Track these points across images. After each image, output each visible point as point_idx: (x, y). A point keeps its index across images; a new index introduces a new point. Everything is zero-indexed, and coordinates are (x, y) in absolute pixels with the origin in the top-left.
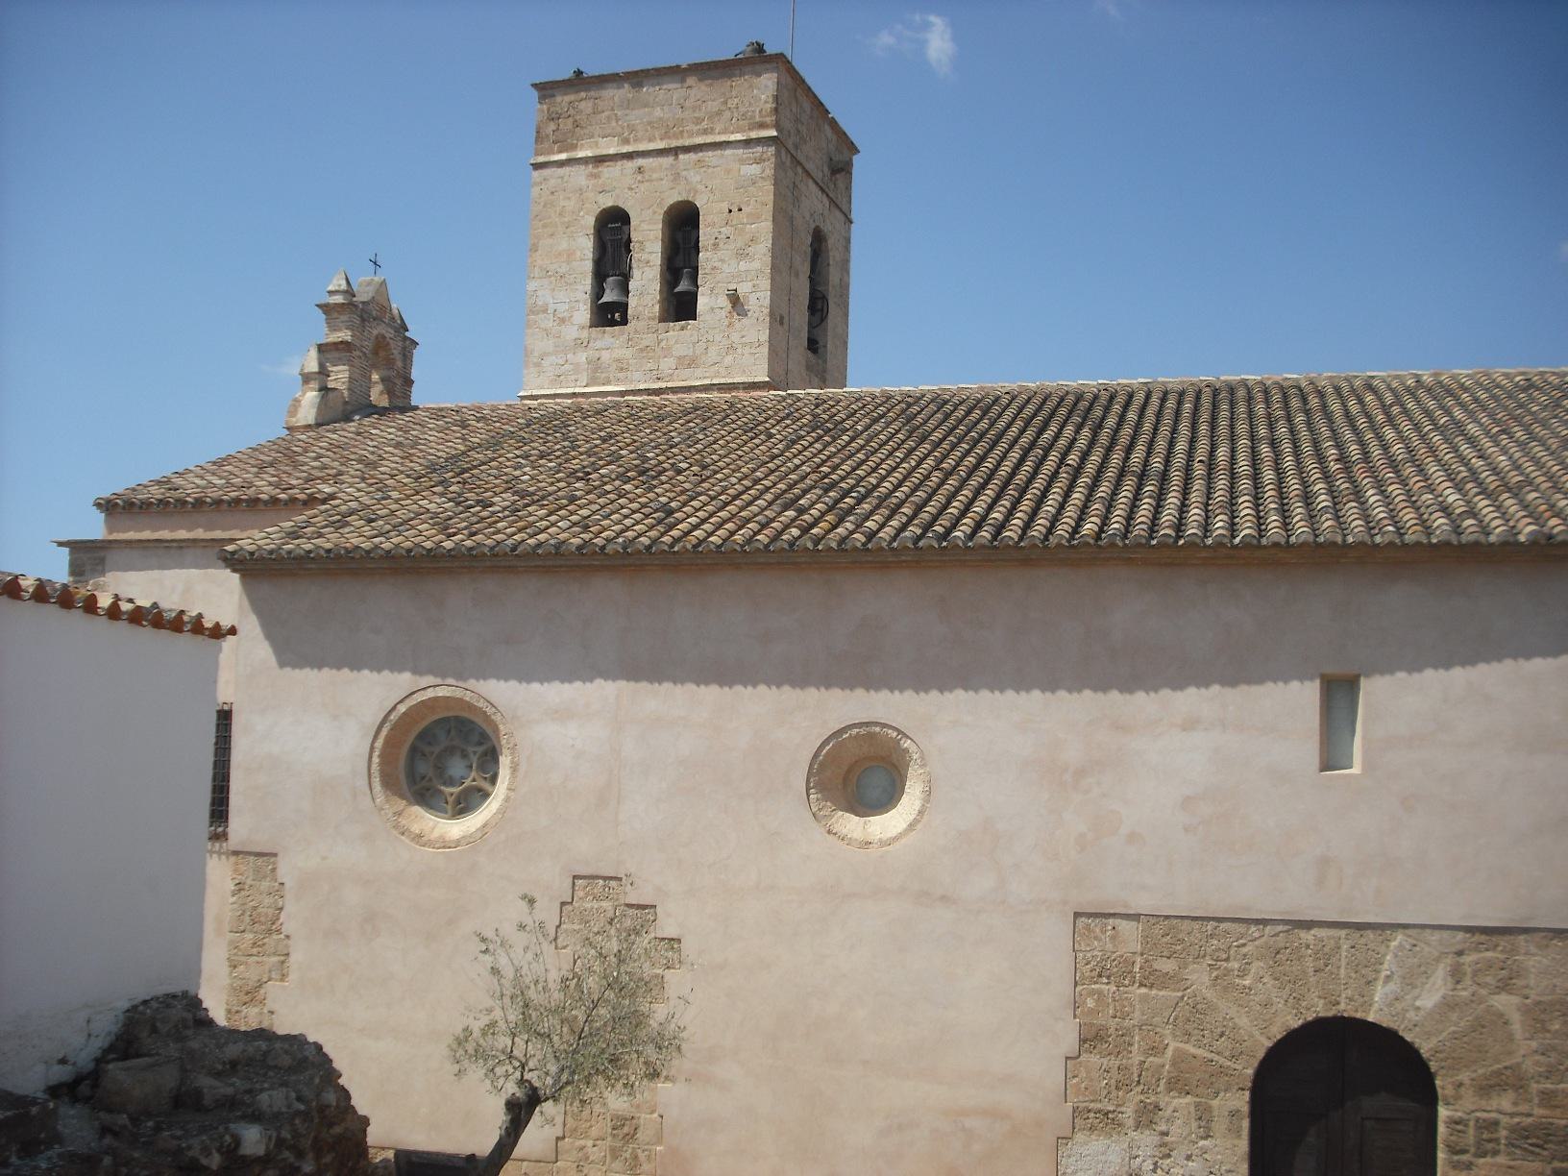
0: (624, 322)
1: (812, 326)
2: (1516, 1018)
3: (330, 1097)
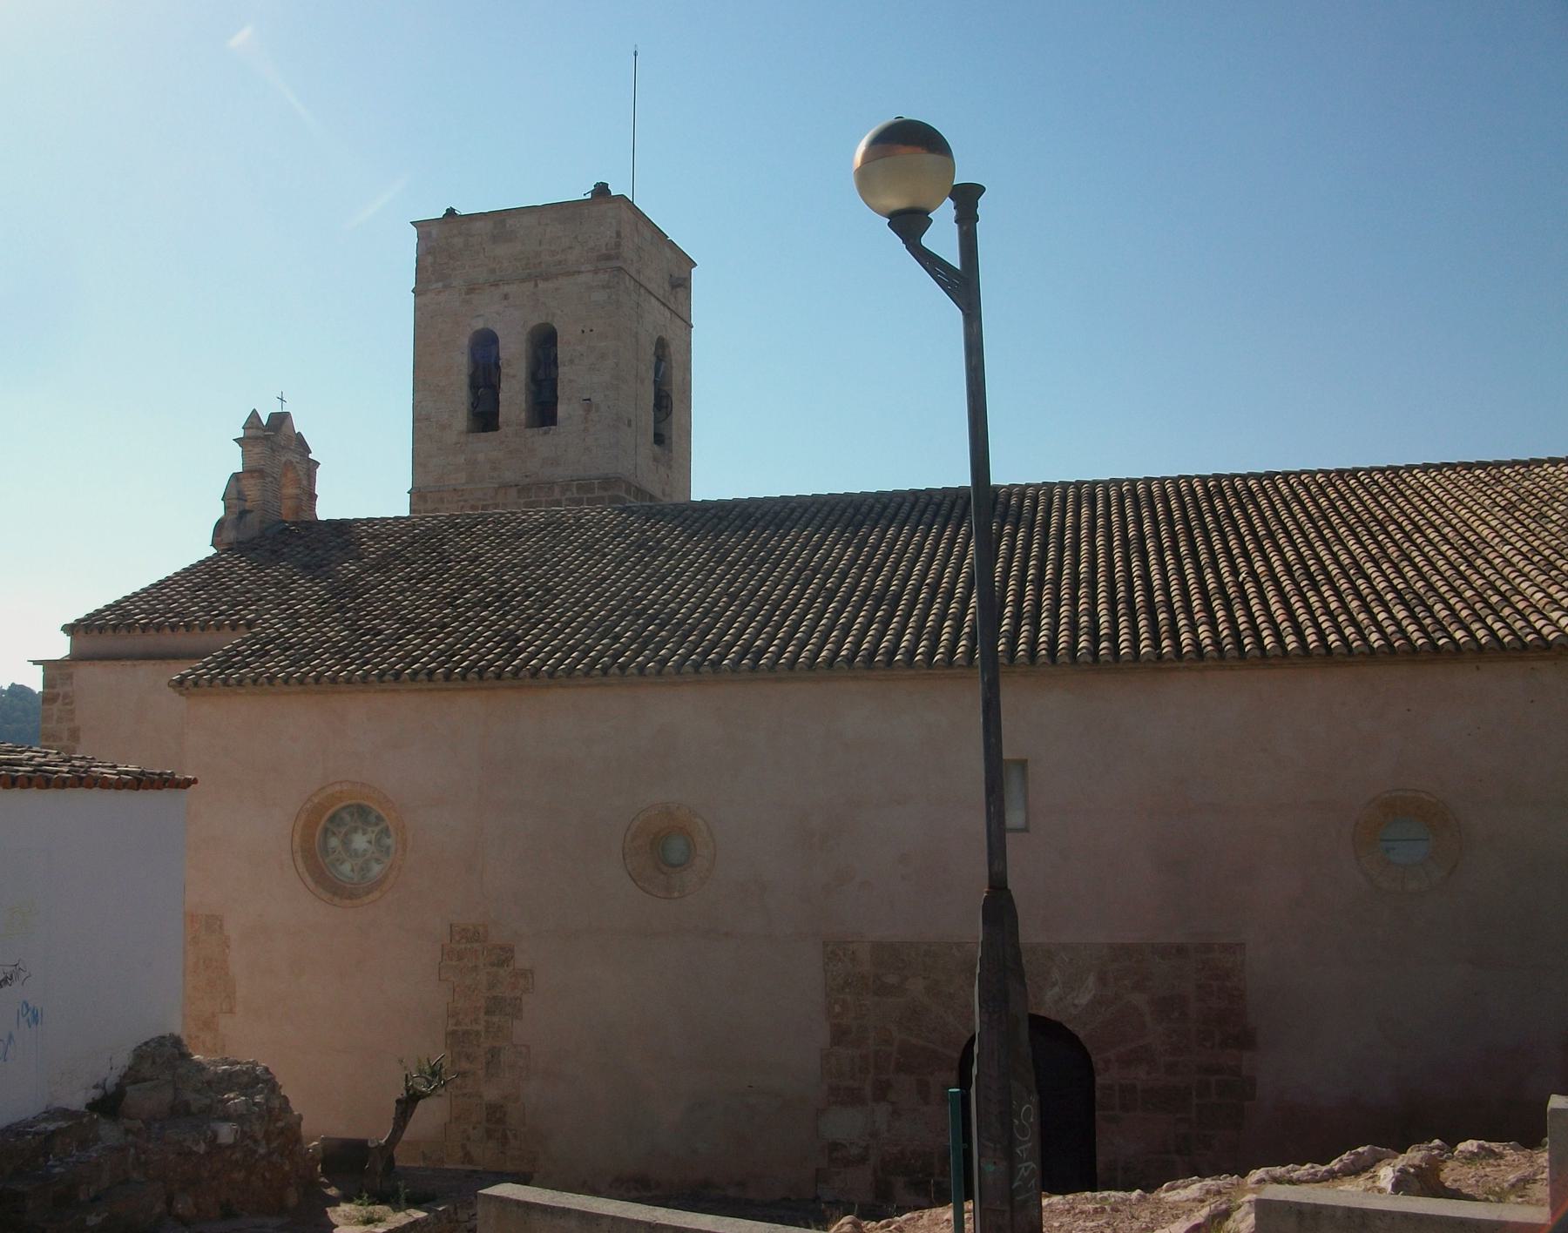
0: (496, 428)
1: (657, 422)
3: (276, 1103)
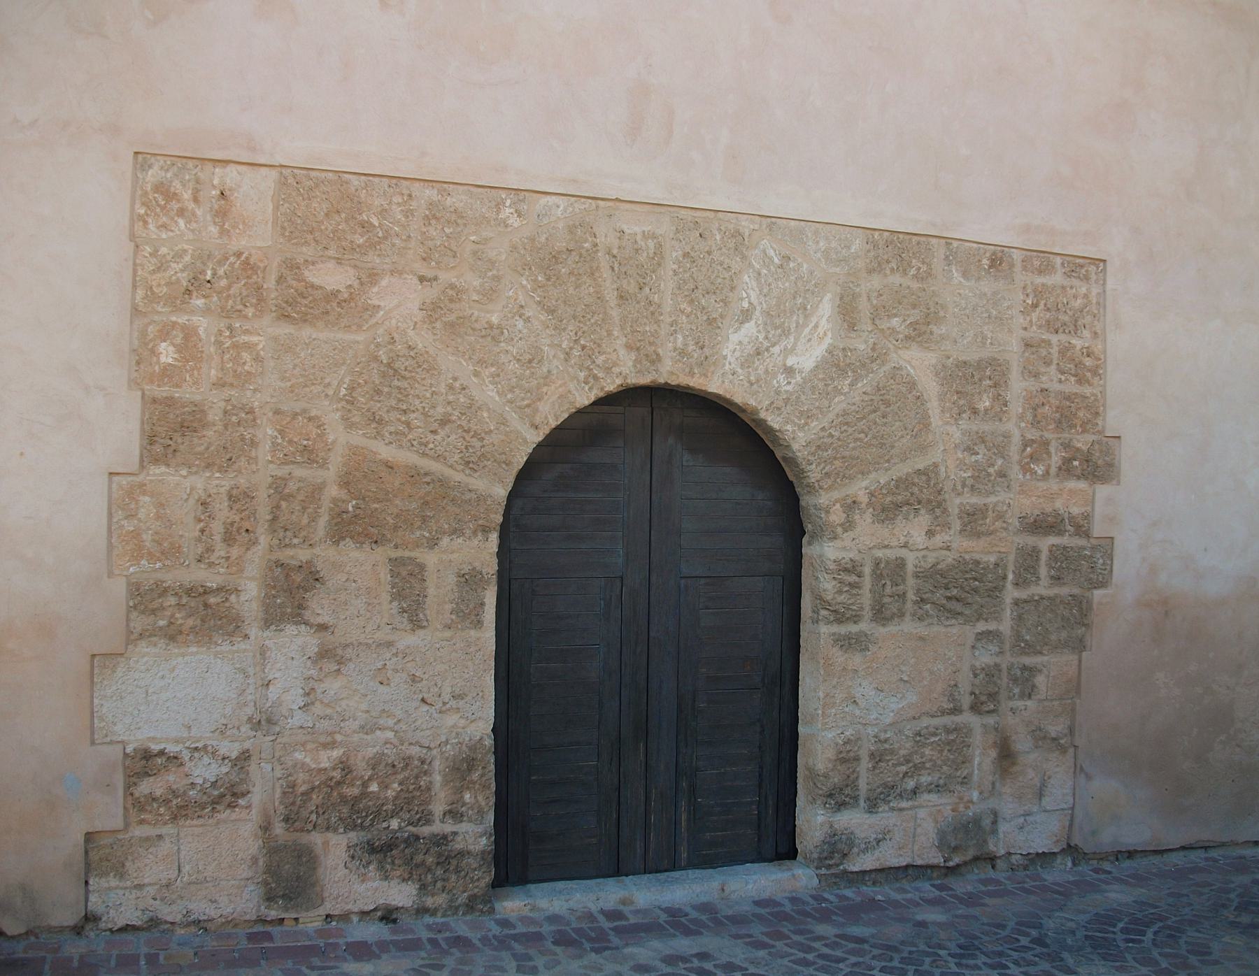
2: (930, 387)
